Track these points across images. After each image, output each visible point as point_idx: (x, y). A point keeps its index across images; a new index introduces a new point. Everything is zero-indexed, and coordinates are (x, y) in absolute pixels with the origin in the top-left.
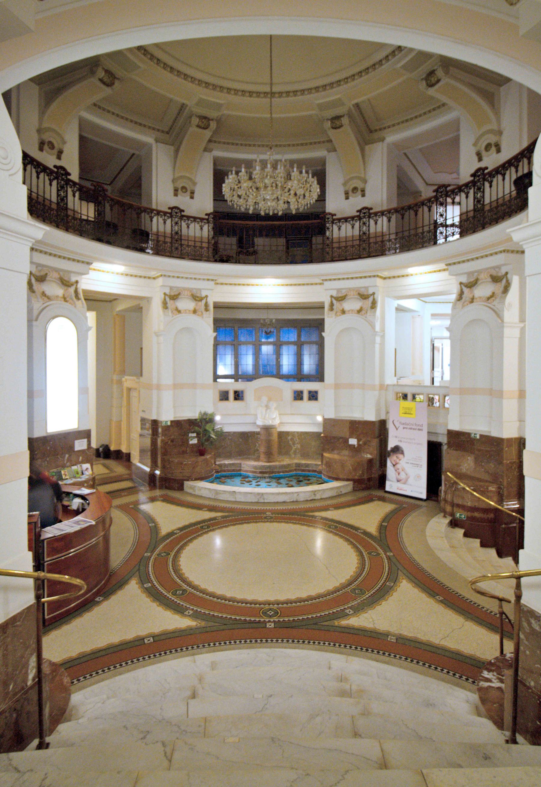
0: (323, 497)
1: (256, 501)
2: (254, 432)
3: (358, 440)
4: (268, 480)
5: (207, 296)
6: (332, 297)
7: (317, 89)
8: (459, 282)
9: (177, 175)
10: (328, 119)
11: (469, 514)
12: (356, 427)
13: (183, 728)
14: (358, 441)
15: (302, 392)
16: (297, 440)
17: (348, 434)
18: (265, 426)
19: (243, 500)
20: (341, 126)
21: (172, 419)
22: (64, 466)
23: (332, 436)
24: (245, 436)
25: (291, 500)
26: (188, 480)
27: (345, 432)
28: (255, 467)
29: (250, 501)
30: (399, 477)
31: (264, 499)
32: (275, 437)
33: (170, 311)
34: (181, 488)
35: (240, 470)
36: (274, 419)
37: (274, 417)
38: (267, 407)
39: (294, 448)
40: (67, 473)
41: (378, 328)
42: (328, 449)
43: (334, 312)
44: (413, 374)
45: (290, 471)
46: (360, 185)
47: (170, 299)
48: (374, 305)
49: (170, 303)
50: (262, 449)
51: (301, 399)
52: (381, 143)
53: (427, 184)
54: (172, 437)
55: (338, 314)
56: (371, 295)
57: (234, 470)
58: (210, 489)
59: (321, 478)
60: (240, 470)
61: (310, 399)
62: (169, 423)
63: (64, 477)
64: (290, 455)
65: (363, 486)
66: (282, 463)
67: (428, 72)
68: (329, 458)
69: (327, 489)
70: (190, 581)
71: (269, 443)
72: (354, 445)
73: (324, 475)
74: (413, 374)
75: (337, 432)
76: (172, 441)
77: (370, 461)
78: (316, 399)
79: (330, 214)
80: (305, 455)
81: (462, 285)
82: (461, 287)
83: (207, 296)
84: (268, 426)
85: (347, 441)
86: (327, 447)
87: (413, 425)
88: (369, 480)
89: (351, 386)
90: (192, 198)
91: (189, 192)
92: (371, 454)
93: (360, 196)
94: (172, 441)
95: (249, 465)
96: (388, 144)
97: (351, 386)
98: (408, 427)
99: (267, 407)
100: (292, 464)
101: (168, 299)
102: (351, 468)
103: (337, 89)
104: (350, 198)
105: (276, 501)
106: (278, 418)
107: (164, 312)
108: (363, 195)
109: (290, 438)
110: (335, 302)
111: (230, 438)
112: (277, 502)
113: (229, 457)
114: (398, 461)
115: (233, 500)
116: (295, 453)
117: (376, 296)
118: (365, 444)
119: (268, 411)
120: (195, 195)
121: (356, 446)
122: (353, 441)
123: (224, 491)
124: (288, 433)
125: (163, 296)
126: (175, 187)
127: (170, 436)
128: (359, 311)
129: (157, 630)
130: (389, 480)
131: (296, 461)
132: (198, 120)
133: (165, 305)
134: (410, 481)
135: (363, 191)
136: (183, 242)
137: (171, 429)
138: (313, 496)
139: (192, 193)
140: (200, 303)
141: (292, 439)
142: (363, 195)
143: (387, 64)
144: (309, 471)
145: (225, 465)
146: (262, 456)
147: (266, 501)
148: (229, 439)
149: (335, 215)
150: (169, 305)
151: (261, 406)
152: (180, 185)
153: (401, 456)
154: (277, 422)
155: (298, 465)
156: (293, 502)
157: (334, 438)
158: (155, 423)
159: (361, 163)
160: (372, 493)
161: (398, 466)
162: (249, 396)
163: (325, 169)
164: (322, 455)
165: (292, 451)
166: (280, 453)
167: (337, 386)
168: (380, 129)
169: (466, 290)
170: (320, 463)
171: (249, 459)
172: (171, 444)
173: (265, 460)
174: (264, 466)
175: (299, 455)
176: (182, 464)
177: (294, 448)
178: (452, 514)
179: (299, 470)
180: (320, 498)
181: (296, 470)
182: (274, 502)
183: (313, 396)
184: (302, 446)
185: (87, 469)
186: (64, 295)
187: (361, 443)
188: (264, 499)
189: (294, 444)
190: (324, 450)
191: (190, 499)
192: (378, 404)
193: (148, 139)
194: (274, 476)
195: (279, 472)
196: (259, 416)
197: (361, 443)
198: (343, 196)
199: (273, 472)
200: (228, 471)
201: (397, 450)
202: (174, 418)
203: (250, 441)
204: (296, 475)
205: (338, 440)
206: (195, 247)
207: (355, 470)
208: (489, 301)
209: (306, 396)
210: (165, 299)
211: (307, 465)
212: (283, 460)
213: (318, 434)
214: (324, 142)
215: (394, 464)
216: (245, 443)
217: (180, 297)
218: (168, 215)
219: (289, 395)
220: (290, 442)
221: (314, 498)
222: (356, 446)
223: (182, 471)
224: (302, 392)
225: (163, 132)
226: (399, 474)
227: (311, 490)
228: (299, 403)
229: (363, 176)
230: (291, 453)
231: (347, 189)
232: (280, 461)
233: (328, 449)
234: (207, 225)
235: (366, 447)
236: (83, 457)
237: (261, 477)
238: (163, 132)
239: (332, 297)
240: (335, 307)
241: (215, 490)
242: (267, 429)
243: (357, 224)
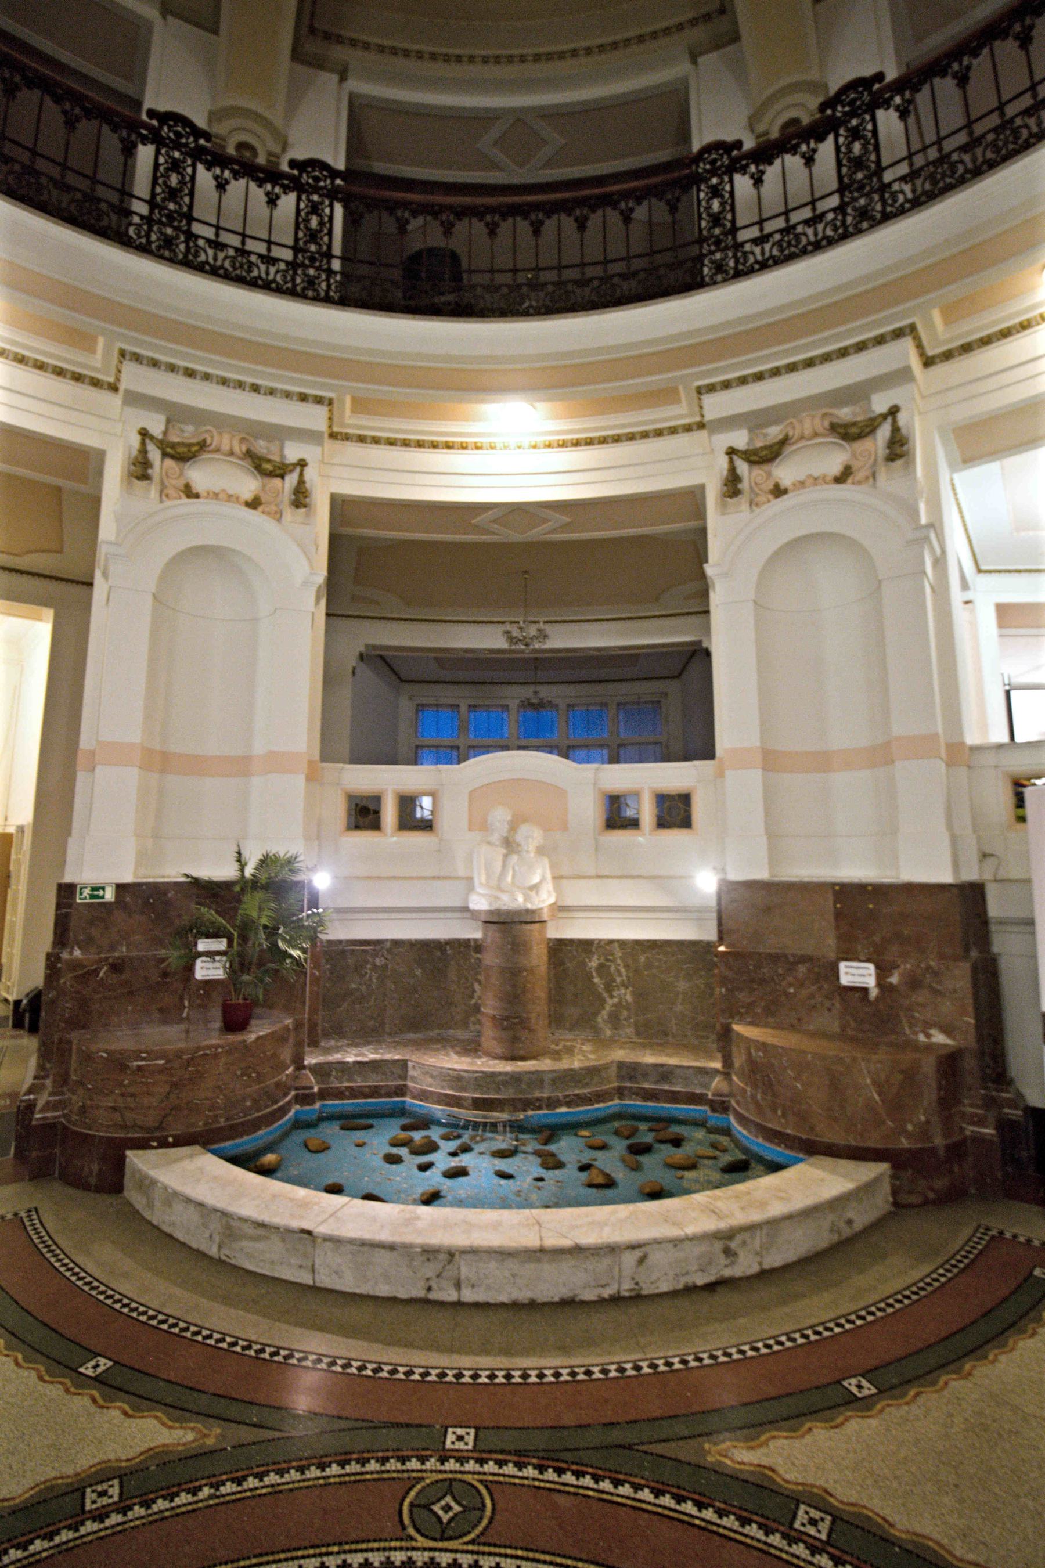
0: (775, 1259)
1: (418, 1292)
2: (465, 943)
3: (878, 967)
4: (502, 1142)
5: (302, 464)
6: (731, 452)
12: (862, 912)
14: (883, 971)
17: (831, 943)
18: (498, 912)
19: (348, 1283)
21: (128, 878)
23: (760, 956)
24: (432, 954)
25: (606, 1293)
26: (142, 1145)
28: (457, 1079)
29: (383, 1290)
31: (458, 1285)
32: (538, 958)
35: (401, 1091)
36: (535, 888)
37: (536, 879)
43: (743, 501)
45: (600, 1097)
47: (165, 455)
50: (491, 1007)
56: (884, 417)
57: (375, 1092)
58: (201, 1205)
59: (727, 1131)
60: (401, 1091)
61: (663, 823)
62: (109, 895)
64: (597, 1031)
65: (941, 1183)
66: (565, 1064)
68: (764, 1046)
69: (789, 1217)
71: (514, 977)
72: (865, 990)
73: (742, 1119)
76: (116, 967)
77: (950, 1063)
78: (686, 823)
80: (652, 1033)
83: (302, 464)
84: (508, 912)
88: (957, 1150)
89: (822, 762)
92: (947, 1031)
95: (438, 1067)
97: (822, 762)
99: (510, 845)
100: (607, 1067)
105: (523, 1295)
106: (548, 886)
110: (742, 467)
112: (532, 1305)
113: (368, 1035)
115: (305, 1278)
116: (614, 1020)
117: (902, 418)
118: (914, 983)
119: (515, 858)
121: (874, 993)
123: (262, 1225)
124: (586, 945)
125: (135, 441)
127: (112, 948)
131: (620, 1054)
136: (197, 228)
137: (119, 915)
138: (723, 1260)
140: (277, 482)
141: (601, 967)
144: (674, 1097)
145: (344, 1068)
146: (489, 1035)
147: (468, 1295)
148: (375, 967)
150: (156, 471)
151: (489, 843)
154: (544, 900)
155: (630, 1071)
156: (616, 1300)
157: (775, 958)
158: (66, 891)
160: (996, 1224)
162: (453, 819)
164: (727, 1031)
166: (556, 1020)
167: (771, 760)
170: (718, 1065)
171: (444, 1043)
173: (499, 1051)
174: (493, 1075)
175: (630, 1031)
180: (755, 1269)
181: (620, 1092)
182: (515, 1306)
183: (675, 811)
187: (894, 979)
188: (458, 1285)
189: (609, 988)
190: (733, 1011)
194: (528, 1123)
195: (552, 1103)
196: (480, 878)
197: (894, 979)
199: (527, 1104)
200: (354, 1093)
203: (452, 975)
204: (619, 1116)
206: (242, 252)
207: (896, 1106)
210: (143, 451)
211: (665, 1073)
212: (570, 1051)
213: (695, 952)
214: (680, 27)
216: (426, 983)
219: (589, 811)
220: (596, 980)
221: (727, 1273)
222: (874, 993)
223: (121, 1102)
227: (710, 1225)
232: (556, 1055)
233: (750, 1006)
234: (292, 196)
235: (922, 996)
237: (476, 1126)
239: (731, 452)
240: (744, 486)
241: (224, 1214)
242: (509, 925)
243: (826, 150)
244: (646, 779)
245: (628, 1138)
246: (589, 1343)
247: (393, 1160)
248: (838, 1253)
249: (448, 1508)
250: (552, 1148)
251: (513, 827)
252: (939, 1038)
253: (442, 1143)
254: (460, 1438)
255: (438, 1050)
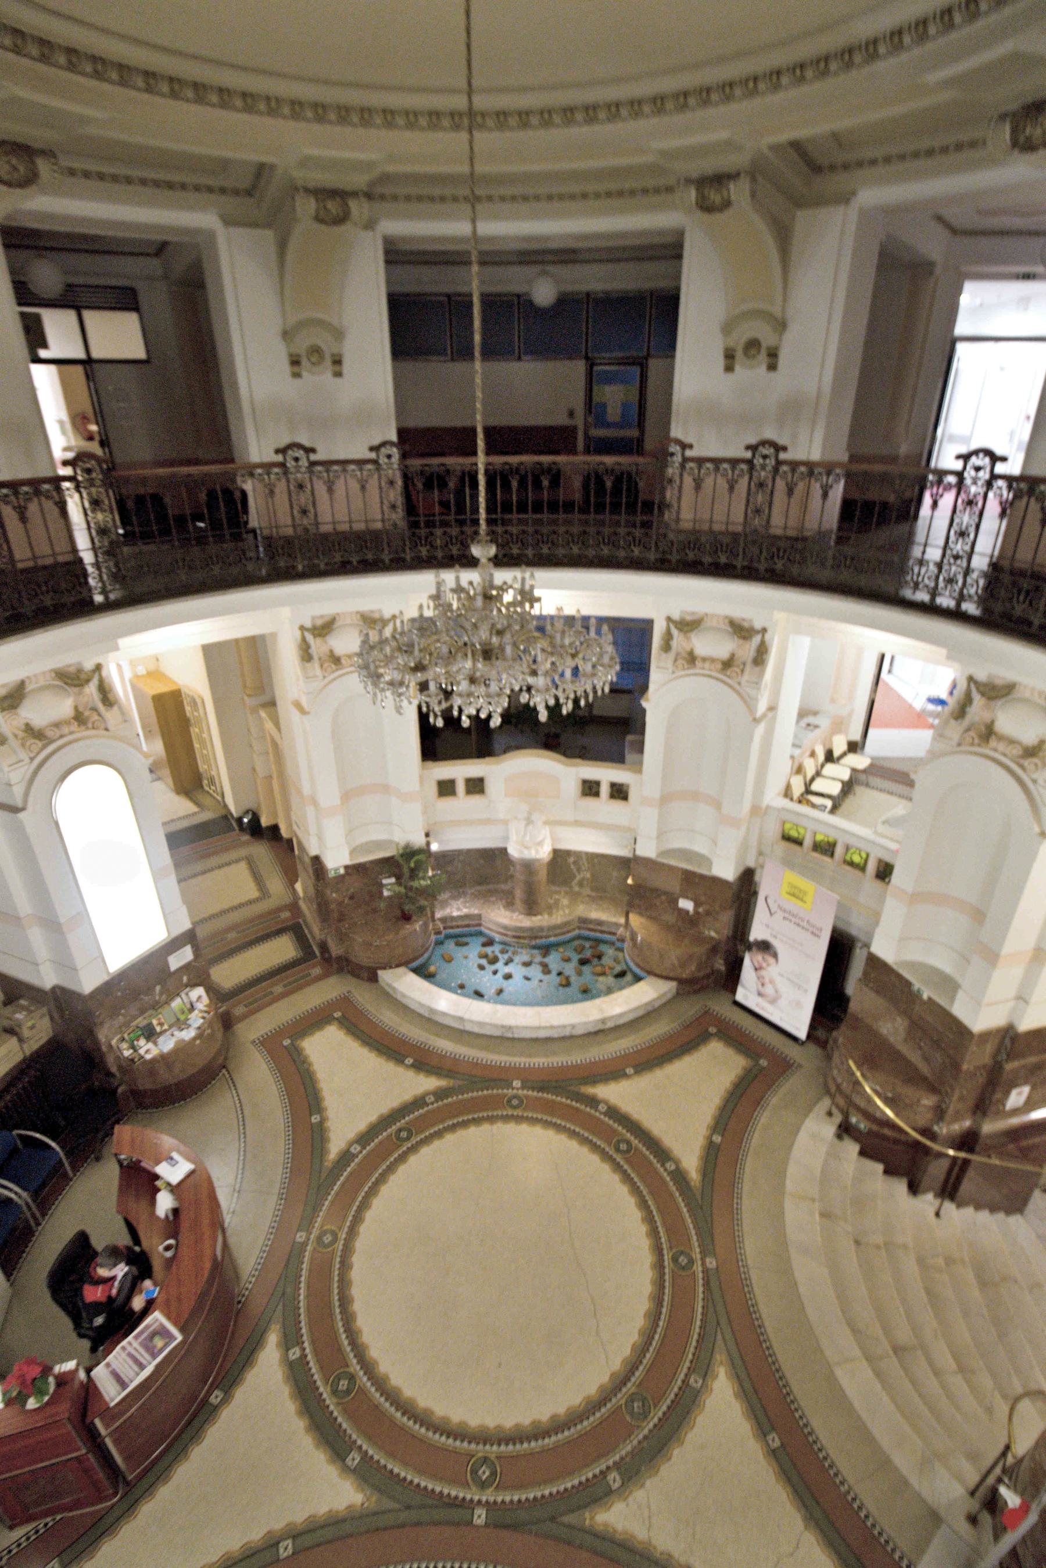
7: (659, 103)
8: (967, 674)
9: (292, 320)
10: (689, 181)
11: (875, 1128)
12: (696, 882)
13: (450, 945)
14: (697, 905)
15: (598, 783)
16: (584, 864)
20: (727, 204)
21: (348, 862)
22: (156, 1006)
26: (384, 968)
27: (674, 885)
30: (762, 990)
33: (316, 664)
34: (373, 978)
35: (480, 925)
38: (529, 821)
39: (578, 877)
40: (163, 1020)
41: (762, 707)
42: (639, 906)
44: (833, 700)
46: (768, 338)
47: (315, 636)
48: (760, 657)
49: (317, 646)
51: (597, 794)
52: (843, 207)
53: (954, 231)
54: (350, 893)
55: (680, 662)
60: (480, 925)
62: (342, 871)
63: (158, 1029)
67: (1030, 100)
70: (363, 1344)
72: (687, 912)
74: (833, 700)
75: (659, 882)
76: (351, 898)
79: (678, 442)
81: (972, 686)
82: (969, 685)
85: (675, 902)
86: (637, 902)
87: (803, 920)
89: (695, 796)
90: (338, 374)
91: (328, 362)
93: (764, 367)
94: (351, 898)
96: (863, 213)
98: (793, 919)
101: (309, 637)
102: (676, 962)
103: (723, 109)
104: (737, 368)
107: (304, 669)
108: (772, 367)
109: (571, 860)
110: (675, 632)
111: (461, 858)
114: (764, 965)
117: (767, 636)
118: (708, 913)
119: (531, 827)
120: (346, 368)
122: (686, 904)
125: (298, 633)
126: (291, 355)
127: (348, 890)
128: (727, 664)
129: (299, 1516)
130: (743, 986)
132: (313, 201)
133: (306, 654)
134: (783, 1002)
135: (773, 354)
139: (337, 361)
141: (574, 862)
142: (772, 367)
143: (892, 61)
144: (602, 932)
147: (516, 1036)
148: (459, 861)
149: (691, 446)
152: (301, 346)
153: (771, 960)
159: (779, 286)
161: (763, 973)
163: (678, 289)
165: (576, 881)
168: (846, 167)
169: (977, 699)
172: (351, 902)
176: (371, 945)
177: (578, 877)
178: (846, 1116)
179: (584, 929)
183: (619, 792)
184: (593, 875)
185: (200, 997)
186: (76, 708)
187: (701, 910)
189: (579, 870)
191: (388, 1018)
192: (744, 847)
193: (197, 218)
197: (701, 910)
198: (721, 362)
199: (536, 938)
200: (458, 927)
201: (765, 946)
202: (353, 852)
205: (659, 896)
207: (683, 965)
208: (1026, 763)
209: (605, 790)
215: (757, 965)
217: (335, 626)
218: (276, 470)
224: (598, 783)
225: (236, 192)
226: (763, 985)
228: (591, 801)
229: (777, 310)
230: (573, 884)
231: (732, 345)
235: (710, 919)
236: (189, 975)
238: (236, 192)
244: (605, 774)
245: (580, 953)
246: (555, 1054)
247: (482, 968)
248: (648, 1015)
249: (515, 1102)
250: (546, 960)
251: (530, 813)
252: (713, 934)
253: (500, 956)
254: (517, 1084)
255: (493, 903)
